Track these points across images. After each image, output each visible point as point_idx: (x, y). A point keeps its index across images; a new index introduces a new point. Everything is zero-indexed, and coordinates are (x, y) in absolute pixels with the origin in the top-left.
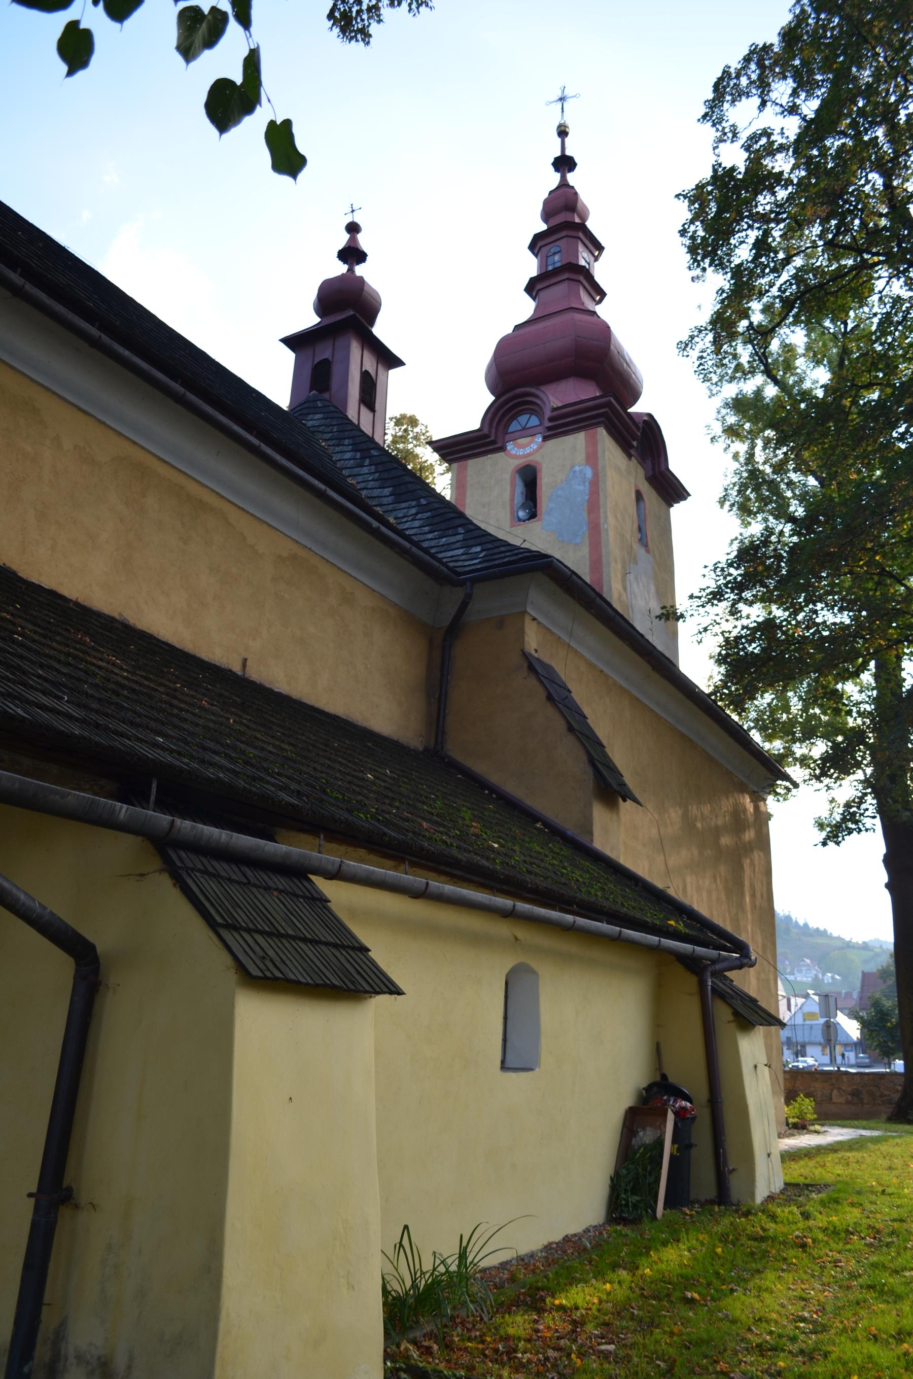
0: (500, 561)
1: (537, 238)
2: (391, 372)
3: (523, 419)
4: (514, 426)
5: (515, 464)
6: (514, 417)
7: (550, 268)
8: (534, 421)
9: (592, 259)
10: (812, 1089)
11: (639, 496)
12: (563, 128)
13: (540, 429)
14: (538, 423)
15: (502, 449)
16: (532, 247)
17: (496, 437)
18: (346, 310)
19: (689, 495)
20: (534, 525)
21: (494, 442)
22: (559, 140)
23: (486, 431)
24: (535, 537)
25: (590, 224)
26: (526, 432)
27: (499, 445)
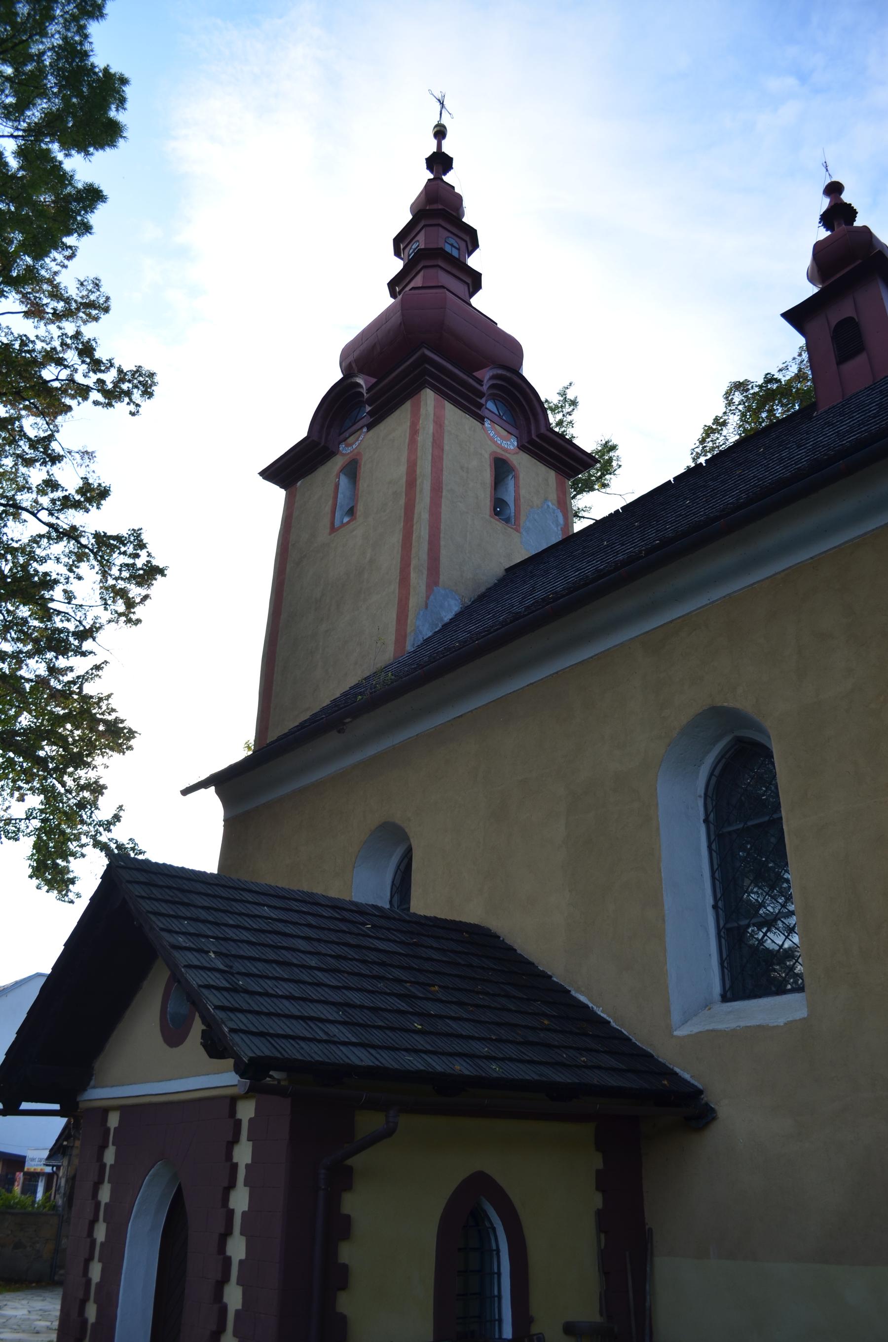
15: (481, 419)
22: (435, 142)
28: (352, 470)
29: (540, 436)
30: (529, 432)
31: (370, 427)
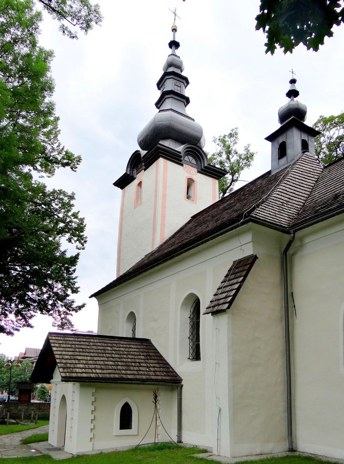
12: (173, 28)
15: (182, 165)
28: (140, 184)
29: (205, 167)
30: (201, 166)
31: (145, 170)
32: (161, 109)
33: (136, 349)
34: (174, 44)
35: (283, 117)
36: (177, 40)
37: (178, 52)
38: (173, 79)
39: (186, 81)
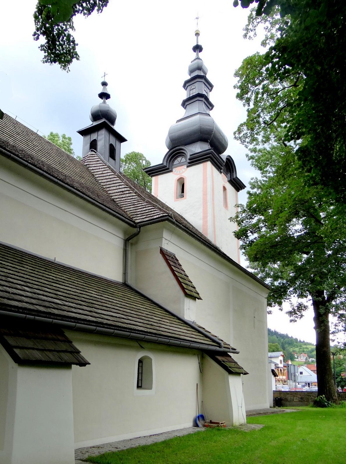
0: (157, 216)
1: (187, 82)
2: (122, 144)
3: (179, 159)
4: (176, 162)
5: (178, 177)
6: (176, 159)
7: (191, 95)
8: (183, 160)
9: (209, 91)
10: (287, 397)
11: (225, 189)
12: (197, 32)
13: (186, 163)
14: (185, 161)
16: (184, 86)
17: (169, 166)
18: (103, 121)
19: (246, 187)
20: (182, 201)
21: (168, 169)
23: (165, 164)
24: (178, 207)
25: (208, 77)
26: (181, 164)
27: (170, 170)
29: (233, 179)
32: (200, 417)
33: (113, 195)
34: (198, 48)
35: (95, 116)
36: (199, 44)
37: (201, 55)
38: (199, 101)
39: (210, 86)
